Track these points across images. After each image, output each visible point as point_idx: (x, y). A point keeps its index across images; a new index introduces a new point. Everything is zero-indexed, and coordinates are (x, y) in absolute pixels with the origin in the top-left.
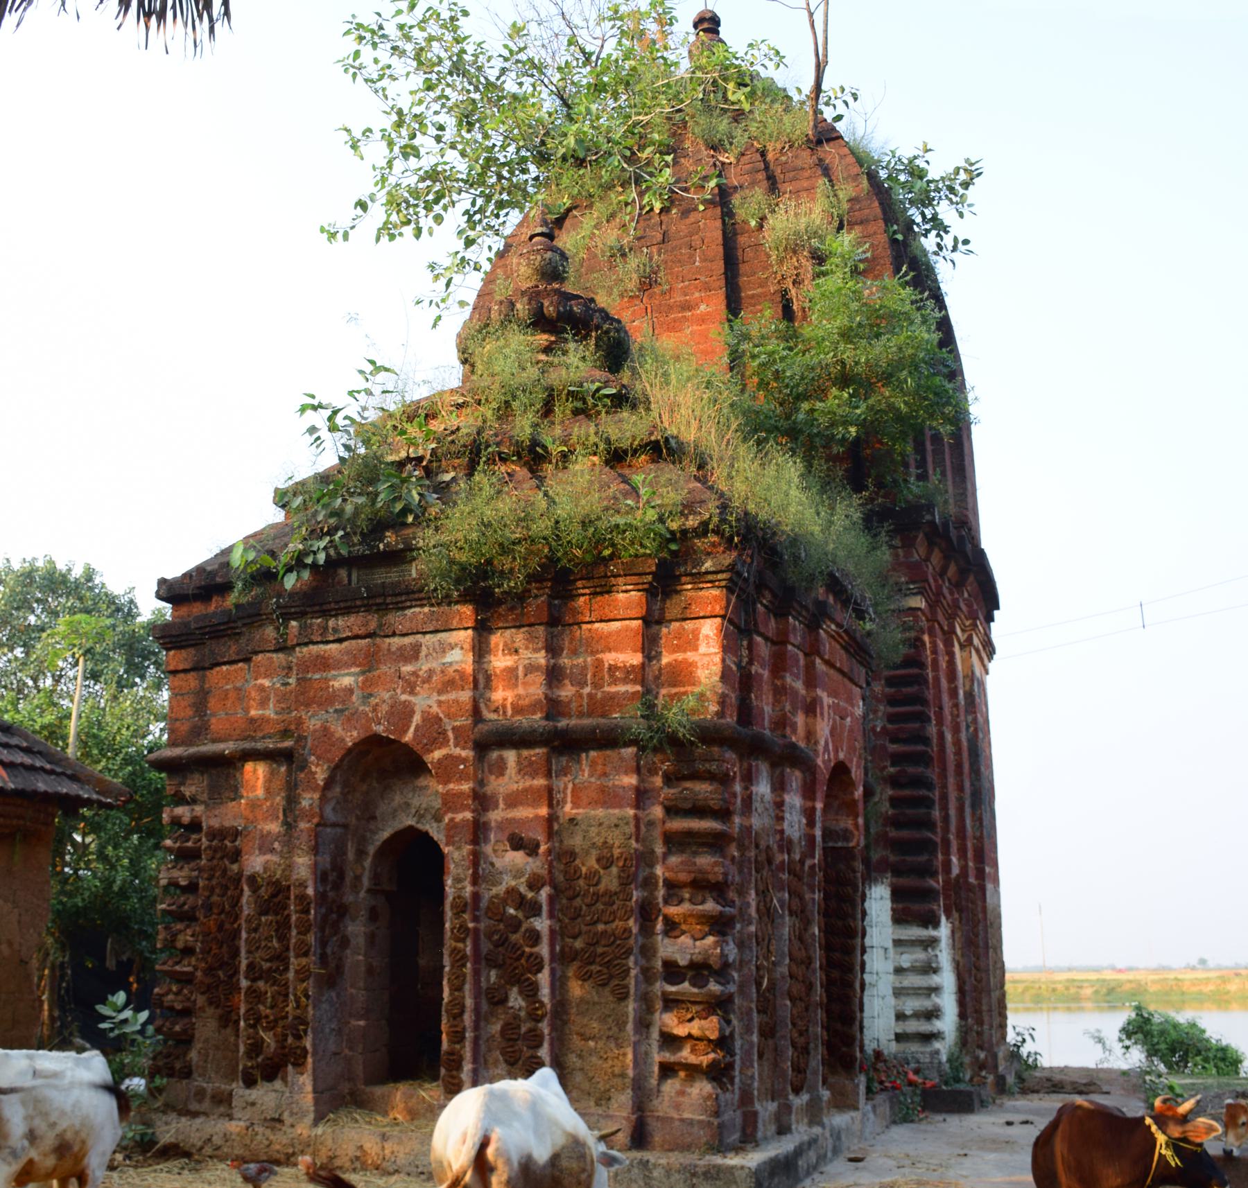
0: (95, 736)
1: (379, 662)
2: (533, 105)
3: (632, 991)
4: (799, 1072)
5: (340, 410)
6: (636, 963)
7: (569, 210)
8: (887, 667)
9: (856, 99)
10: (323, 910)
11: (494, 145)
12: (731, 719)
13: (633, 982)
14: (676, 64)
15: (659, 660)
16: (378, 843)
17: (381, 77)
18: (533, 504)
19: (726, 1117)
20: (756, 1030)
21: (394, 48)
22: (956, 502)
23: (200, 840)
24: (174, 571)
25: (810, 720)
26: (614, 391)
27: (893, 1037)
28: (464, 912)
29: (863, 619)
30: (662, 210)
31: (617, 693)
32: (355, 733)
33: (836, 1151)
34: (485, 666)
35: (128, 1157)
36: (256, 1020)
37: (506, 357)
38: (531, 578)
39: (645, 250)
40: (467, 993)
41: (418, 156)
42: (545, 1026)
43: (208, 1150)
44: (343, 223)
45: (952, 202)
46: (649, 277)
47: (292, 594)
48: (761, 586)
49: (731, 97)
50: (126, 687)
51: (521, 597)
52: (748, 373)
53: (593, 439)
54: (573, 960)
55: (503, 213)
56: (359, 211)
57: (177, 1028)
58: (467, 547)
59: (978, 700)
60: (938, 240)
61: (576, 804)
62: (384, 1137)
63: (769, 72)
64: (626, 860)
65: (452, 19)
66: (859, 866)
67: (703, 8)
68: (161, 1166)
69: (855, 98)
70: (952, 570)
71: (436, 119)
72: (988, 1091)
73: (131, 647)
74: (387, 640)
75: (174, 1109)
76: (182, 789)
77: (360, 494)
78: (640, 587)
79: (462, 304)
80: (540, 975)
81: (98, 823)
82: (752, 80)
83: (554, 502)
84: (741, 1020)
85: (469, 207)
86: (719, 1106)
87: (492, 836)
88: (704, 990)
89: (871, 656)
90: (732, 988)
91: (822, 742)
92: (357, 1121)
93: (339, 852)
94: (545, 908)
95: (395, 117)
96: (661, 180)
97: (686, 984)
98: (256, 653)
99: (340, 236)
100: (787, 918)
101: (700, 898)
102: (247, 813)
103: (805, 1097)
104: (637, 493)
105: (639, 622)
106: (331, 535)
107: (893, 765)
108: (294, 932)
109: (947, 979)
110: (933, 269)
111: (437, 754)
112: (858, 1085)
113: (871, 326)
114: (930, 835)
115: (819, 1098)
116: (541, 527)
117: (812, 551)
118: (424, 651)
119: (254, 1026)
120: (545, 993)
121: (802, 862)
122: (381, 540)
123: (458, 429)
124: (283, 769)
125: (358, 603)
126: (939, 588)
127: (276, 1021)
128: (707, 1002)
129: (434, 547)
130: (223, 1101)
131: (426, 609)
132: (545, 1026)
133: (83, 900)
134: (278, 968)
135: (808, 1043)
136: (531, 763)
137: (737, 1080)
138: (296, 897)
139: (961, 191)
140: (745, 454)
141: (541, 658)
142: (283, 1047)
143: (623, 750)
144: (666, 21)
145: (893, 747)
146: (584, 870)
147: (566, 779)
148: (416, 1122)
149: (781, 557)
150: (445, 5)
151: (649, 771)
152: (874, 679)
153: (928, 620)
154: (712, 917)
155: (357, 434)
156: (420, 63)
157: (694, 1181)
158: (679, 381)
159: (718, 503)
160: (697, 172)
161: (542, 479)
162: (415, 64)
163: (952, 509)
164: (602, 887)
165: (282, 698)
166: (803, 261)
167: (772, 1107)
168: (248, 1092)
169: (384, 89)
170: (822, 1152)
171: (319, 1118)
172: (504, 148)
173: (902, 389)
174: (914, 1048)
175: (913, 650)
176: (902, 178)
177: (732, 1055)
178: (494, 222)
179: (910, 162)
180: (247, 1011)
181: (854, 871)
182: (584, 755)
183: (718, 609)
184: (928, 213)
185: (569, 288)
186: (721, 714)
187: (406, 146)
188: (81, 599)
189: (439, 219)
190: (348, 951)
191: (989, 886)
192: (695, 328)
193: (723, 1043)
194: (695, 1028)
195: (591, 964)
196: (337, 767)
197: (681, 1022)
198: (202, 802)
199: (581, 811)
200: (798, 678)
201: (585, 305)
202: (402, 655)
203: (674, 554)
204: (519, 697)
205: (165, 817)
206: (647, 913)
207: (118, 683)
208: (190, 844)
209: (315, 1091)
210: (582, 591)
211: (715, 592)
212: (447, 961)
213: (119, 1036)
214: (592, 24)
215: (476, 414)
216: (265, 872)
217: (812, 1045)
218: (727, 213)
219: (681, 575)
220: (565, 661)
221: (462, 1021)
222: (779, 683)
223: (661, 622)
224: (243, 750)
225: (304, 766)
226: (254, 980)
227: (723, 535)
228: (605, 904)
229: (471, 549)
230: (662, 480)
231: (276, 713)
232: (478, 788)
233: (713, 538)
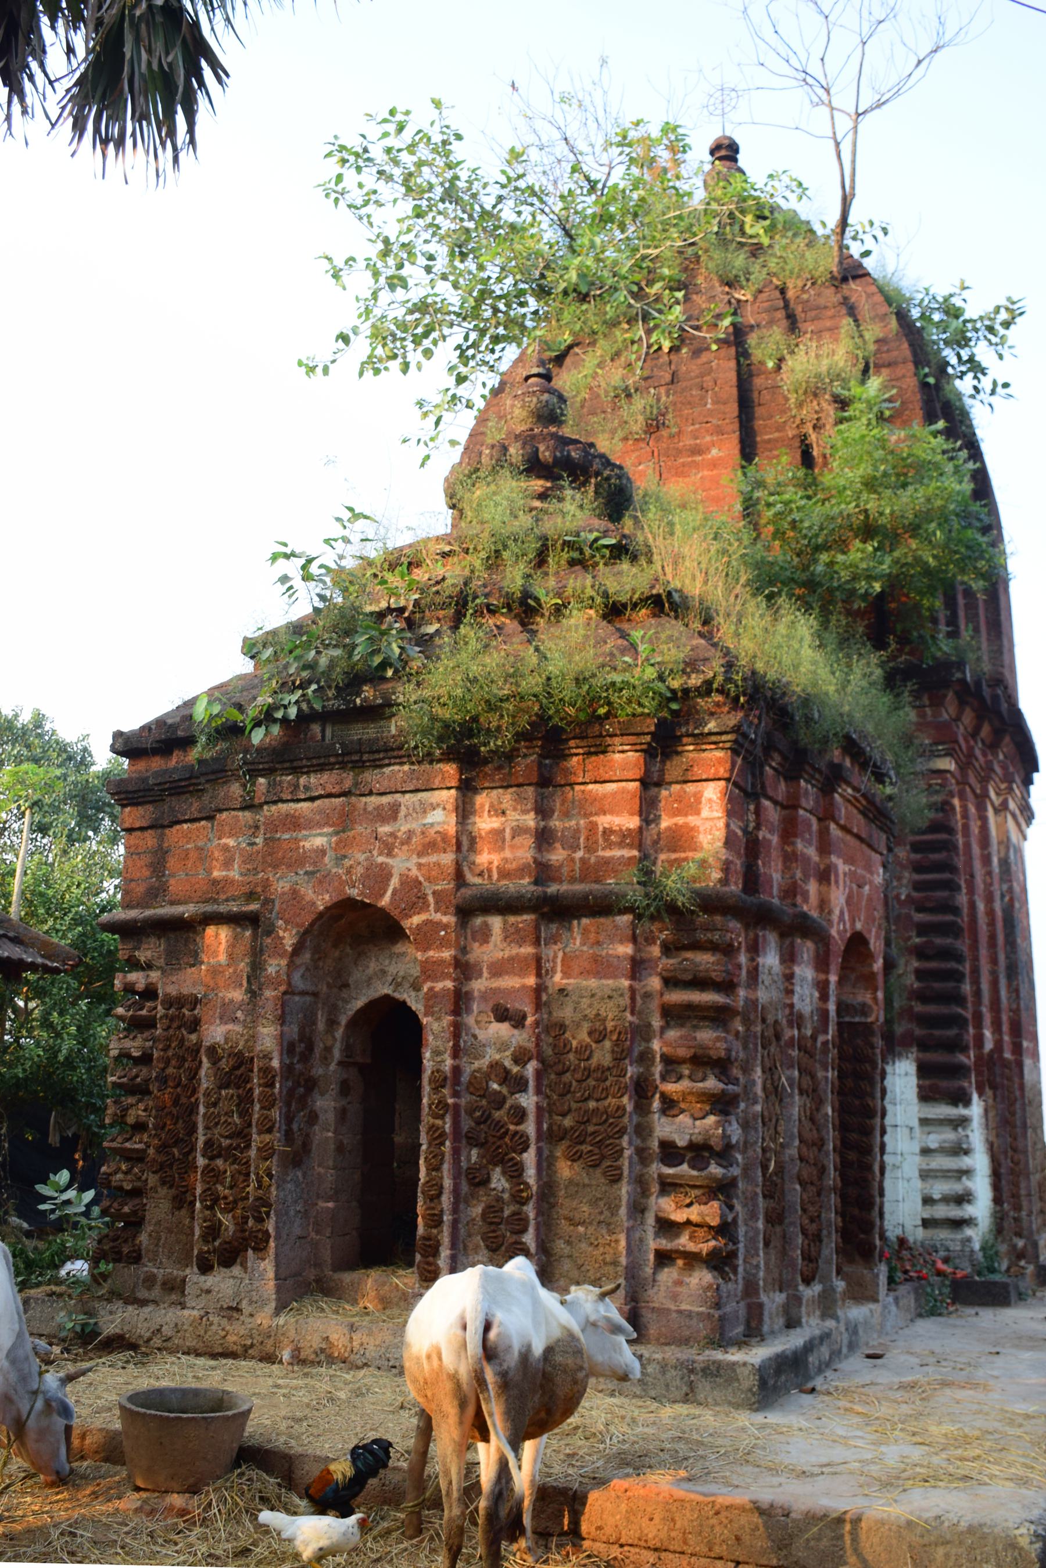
0: (42, 895)
1: (354, 822)
2: (532, 236)
3: (626, 1173)
4: (811, 1260)
5: (314, 559)
6: (630, 1143)
7: (570, 347)
8: (913, 832)
9: (886, 234)
10: (290, 1084)
11: (489, 278)
12: (735, 887)
13: (626, 1163)
14: (689, 194)
15: (658, 824)
16: (351, 1013)
17: (366, 203)
18: (523, 659)
19: (729, 1308)
20: (761, 1217)
21: (381, 173)
22: (990, 659)
23: (155, 1008)
24: (131, 724)
25: (824, 888)
26: (613, 541)
27: (920, 1223)
28: (443, 1087)
29: (883, 782)
30: (671, 349)
31: (612, 858)
32: (327, 897)
33: (852, 1346)
34: (470, 827)
35: (67, 1350)
36: (213, 1201)
38: (519, 736)
39: (652, 391)
40: (445, 1173)
41: (405, 287)
42: (530, 1211)
43: (157, 1342)
44: (322, 358)
45: (991, 343)
46: (656, 419)
47: (260, 750)
48: (769, 748)
49: (749, 231)
50: (78, 841)
51: (510, 756)
52: (763, 521)
53: (590, 592)
54: (562, 1139)
55: (498, 348)
56: (341, 344)
57: (126, 1209)
58: (450, 703)
59: (1014, 868)
60: (975, 382)
61: (566, 974)
62: (352, 1328)
63: (789, 202)
64: (620, 1033)
65: (445, 143)
66: (879, 1042)
67: (720, 134)
68: (103, 1360)
69: (885, 231)
70: (986, 730)
71: (426, 248)
72: (1027, 1282)
73: (83, 798)
74: (364, 799)
75: (119, 1296)
76: (137, 953)
77: (335, 646)
78: (638, 747)
79: (453, 443)
80: (525, 1155)
81: (43, 988)
82: (772, 212)
83: (546, 658)
84: (745, 1205)
85: (461, 341)
86: (720, 1298)
87: (475, 1007)
88: (704, 1173)
89: (892, 822)
90: (736, 1171)
91: (837, 912)
92: (323, 1310)
93: (309, 1021)
94: (531, 1084)
95: (380, 246)
96: (670, 317)
97: (685, 1167)
98: (220, 811)
99: (319, 370)
100: (797, 1098)
101: (700, 1075)
102: (208, 980)
103: (817, 1288)
104: (636, 649)
105: (637, 784)
106: (303, 689)
107: (919, 935)
108: (257, 1107)
109: (980, 1161)
110: (968, 414)
111: (416, 920)
112: (877, 1276)
113: (898, 475)
114: (960, 1010)
115: (833, 1290)
116: (531, 683)
118: (403, 811)
119: (211, 1208)
120: (530, 1174)
121: (814, 1038)
122: (358, 695)
123: (444, 579)
124: (248, 933)
125: (332, 760)
126: (971, 749)
127: (235, 1202)
128: (707, 1187)
129: (415, 703)
130: (175, 1288)
131: (406, 768)
132: (530, 1211)
133: (25, 1070)
134: (239, 1145)
135: (820, 1230)
136: (518, 931)
137: (741, 1269)
138: (260, 1070)
139: (1002, 331)
140: (755, 610)
141: (530, 820)
142: (243, 1231)
143: (618, 918)
144: (678, 147)
145: (919, 917)
146: (574, 1043)
147: (556, 947)
148: (388, 1312)
149: (792, 718)
150: (437, 127)
151: (646, 940)
152: (898, 844)
153: (958, 783)
154: (713, 1095)
156: (409, 190)
157: (692, 1377)
158: (684, 532)
159: (722, 661)
160: (709, 310)
161: (534, 633)
162: (403, 190)
163: (986, 667)
164: (594, 1062)
165: (248, 859)
166: (825, 405)
167: (780, 1298)
168: (203, 1278)
169: (369, 216)
170: (836, 1347)
171: (281, 1307)
172: (499, 280)
173: (930, 542)
174: (943, 1234)
175: (941, 815)
176: (936, 317)
177: (735, 1241)
178: (490, 358)
179: (946, 300)
180: (204, 1191)
181: (873, 1047)
182: (575, 922)
183: (722, 772)
184: (965, 354)
185: (567, 431)
186: (724, 881)
187: (392, 277)
188: (28, 747)
189: (428, 353)
190: (316, 1128)
191: (1028, 1062)
192: (706, 473)
193: (725, 1229)
194: (694, 1213)
195: (581, 1143)
196: (306, 932)
197: (679, 1207)
198: (158, 968)
199: (572, 981)
200: (810, 844)
201: (584, 450)
202: (379, 815)
203: (673, 713)
204: (506, 860)
205: (117, 983)
206: (642, 1090)
207: (69, 836)
208: (144, 1012)
209: (277, 1278)
210: (574, 751)
211: (720, 754)
212: (424, 1139)
213: (60, 1218)
214: (598, 149)
215: (463, 564)
216: (226, 1043)
217: (825, 1232)
218: (742, 353)
219: (682, 736)
220: (556, 823)
221: (440, 1203)
222: (789, 849)
223: (659, 784)
224: (204, 913)
225: (270, 931)
226: (212, 1158)
227: (728, 695)
228: (597, 1080)
229: (455, 705)
230: (663, 636)
231: (241, 874)
232: (460, 956)
233: (717, 698)
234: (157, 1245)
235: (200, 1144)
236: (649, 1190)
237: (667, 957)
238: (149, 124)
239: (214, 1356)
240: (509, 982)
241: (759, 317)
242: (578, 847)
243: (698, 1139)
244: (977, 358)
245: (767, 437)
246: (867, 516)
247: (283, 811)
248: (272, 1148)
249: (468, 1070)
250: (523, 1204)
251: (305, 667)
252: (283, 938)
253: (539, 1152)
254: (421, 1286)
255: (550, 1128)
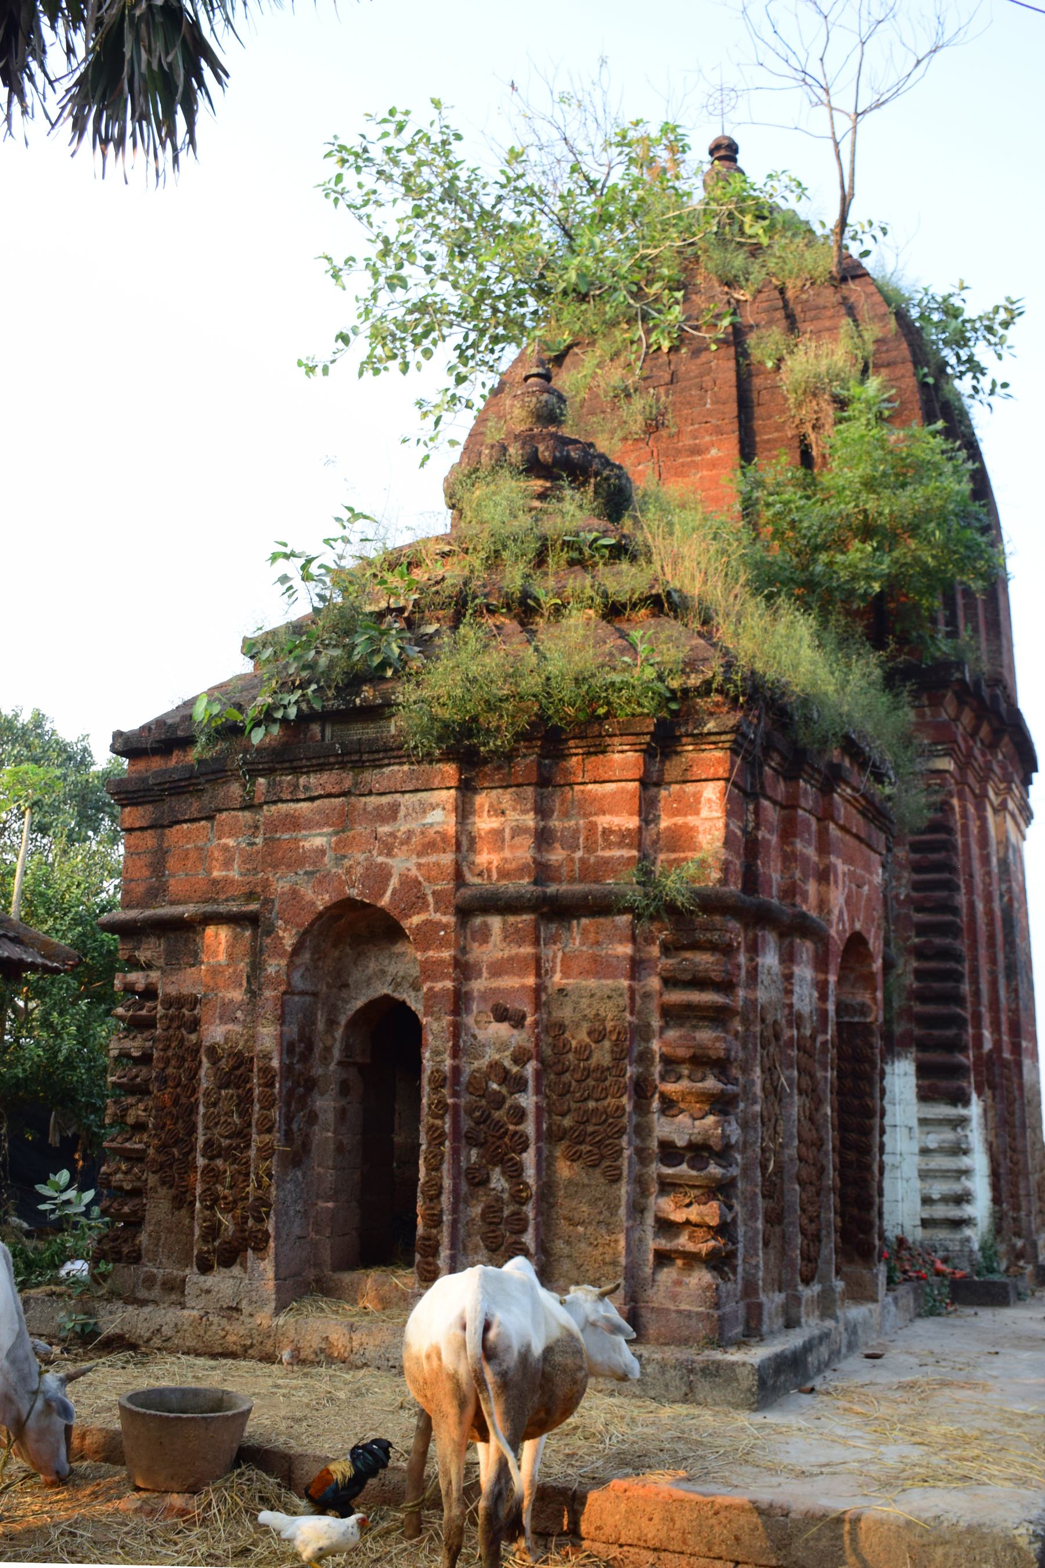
0: (42, 895)
1: (353, 822)
2: (532, 236)
3: (625, 1173)
4: (810, 1260)
5: (314, 559)
6: (630, 1143)
7: (569, 347)
8: (912, 832)
9: (885, 234)
10: (289, 1084)
11: (489, 278)
12: (734, 887)
13: (626, 1163)
14: (689, 194)
15: (657, 824)
16: (350, 1013)
17: (366, 203)
18: (523, 659)
19: (728, 1308)
20: (761, 1217)
21: (380, 173)
22: (989, 659)
23: (155, 1008)
24: (131, 724)
25: (823, 888)
26: (613, 541)
27: (919, 1223)
28: (443, 1087)
29: (882, 782)
30: (670, 349)
31: (612, 858)
32: (327, 897)
33: (851, 1346)
34: (469, 827)
35: (67, 1350)
36: (213, 1201)
37: (496, 505)
38: (519, 736)
39: (652, 391)
40: (445, 1173)
41: (405, 287)
42: (530, 1211)
43: (157, 1342)
44: (322, 358)
45: (990, 343)
46: (656, 419)
47: (259, 750)
48: (768, 748)
49: (748, 231)
50: (78, 841)
51: (509, 756)
52: (762, 521)
53: (589, 592)
54: (561, 1139)
55: (498, 348)
56: (340, 344)
57: (126, 1209)
58: (450, 703)
59: (1013, 868)
60: (974, 382)
61: (566, 974)
62: (352, 1328)
63: (788, 202)
64: (619, 1033)
65: (444, 143)
66: (878, 1042)
67: (719, 134)
68: (103, 1360)
69: (884, 231)
70: (985, 730)
71: (426, 248)
72: (1026, 1282)
73: (83, 798)
74: (363, 799)
75: (119, 1296)
76: (136, 953)
77: (335, 646)
78: (637, 747)
79: (453, 443)
80: (525, 1155)
81: (43, 988)
82: (771, 212)
83: (545, 658)
84: (744, 1205)
85: (460, 341)
86: (720, 1298)
87: (474, 1007)
88: (703, 1173)
89: (891, 822)
90: (735, 1171)
91: (836, 912)
92: (322, 1310)
93: (309, 1021)
94: (531, 1084)
95: (380, 246)
96: (670, 317)
97: (684, 1167)
98: (220, 811)
99: (319, 370)
100: (796, 1098)
101: (700, 1075)
102: (207, 980)
103: (816, 1288)
104: (635, 649)
105: (637, 784)
106: (303, 689)
107: (918, 935)
108: (257, 1107)
109: (979, 1161)
110: (967, 414)
111: (416, 920)
112: (876, 1276)
113: (897, 475)
114: (959, 1010)
115: (832, 1290)
116: (531, 683)
117: (826, 712)
118: (403, 811)
119: (210, 1208)
120: (530, 1174)
121: (813, 1038)
122: (358, 695)
123: (443, 579)
124: (248, 933)
125: (332, 760)
126: (970, 749)
127: (235, 1202)
128: (706, 1187)
129: (415, 703)
130: (175, 1288)
131: (406, 768)
132: (530, 1211)
133: (25, 1070)
134: (238, 1145)
135: (819, 1230)
136: (517, 931)
137: (740, 1269)
138: (260, 1070)
139: (1001, 331)
140: (755, 610)
141: (529, 820)
142: (243, 1231)
143: (617, 918)
144: (677, 147)
145: (918, 917)
146: (574, 1043)
147: (555, 947)
148: (388, 1312)
149: (791, 718)
150: (436, 127)
151: (646, 940)
152: (897, 844)
153: (957, 783)
154: (713, 1095)
155: (335, 583)
156: (409, 190)
157: (692, 1377)
158: (683, 532)
160: (709, 310)
162: (403, 190)
163: (985, 667)
164: (593, 1062)
165: (248, 859)
166: (824, 405)
167: (779, 1298)
168: (203, 1278)
169: (368, 216)
170: (835, 1347)
171: (281, 1307)
172: (499, 280)
173: (929, 542)
174: (942, 1234)
175: (940, 815)
176: (936, 317)
177: (734, 1241)
178: (489, 358)
179: (945, 300)
180: (204, 1191)
181: (872, 1047)
182: (575, 922)
183: (721, 772)
184: (964, 354)
185: (566, 431)
186: (723, 881)
187: (391, 277)
188: (28, 747)
189: (427, 353)
190: (316, 1128)
191: (1027, 1062)
192: (705, 473)
193: (724, 1229)
194: (693, 1213)
195: (581, 1143)
196: (306, 932)
197: (678, 1207)
198: (158, 968)
199: (571, 981)
200: (810, 844)
201: (584, 450)
202: (379, 815)
203: (673, 713)
204: (505, 860)
205: (117, 983)
206: (642, 1090)
207: (69, 836)
208: (144, 1012)
209: (277, 1278)
210: (574, 751)
211: (719, 754)
212: (423, 1139)
213: (60, 1218)
214: (598, 149)
215: (463, 564)
216: (226, 1043)
217: (824, 1232)
218: (742, 353)
219: (681, 736)
220: (555, 823)
221: (440, 1203)
222: (788, 849)
223: (658, 784)
224: (204, 913)
225: (270, 931)
226: (211, 1158)
227: (727, 695)
228: (596, 1080)
229: (455, 705)
230: (662, 636)
231: (241, 874)
232: (459, 956)
233: (717, 698)
234: (157, 1245)
235: (200, 1144)
236: (648, 1190)
237: (667, 957)
238: (149, 124)
239: (214, 1356)
240: (509, 982)
241: (758, 317)
242: (578, 847)
243: (697, 1139)
244: (976, 358)
245: (766, 437)
246: (866, 516)
247: (283, 811)
248: (272, 1148)
249: (467, 1070)
250: (523, 1204)
251: (305, 667)
252: (283, 938)
253: (539, 1152)
254: (421, 1286)
255: (549, 1128)
